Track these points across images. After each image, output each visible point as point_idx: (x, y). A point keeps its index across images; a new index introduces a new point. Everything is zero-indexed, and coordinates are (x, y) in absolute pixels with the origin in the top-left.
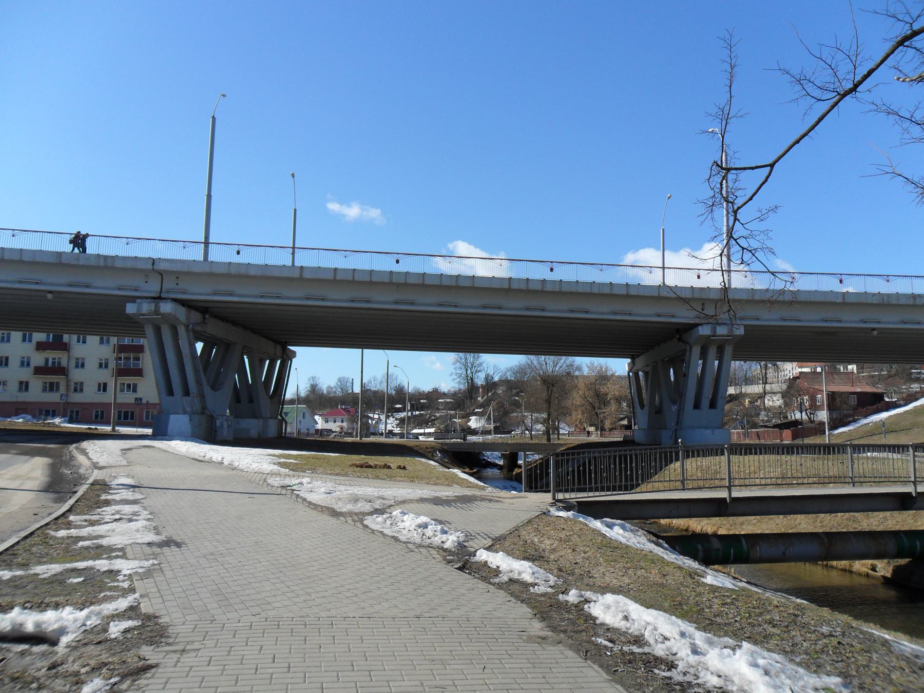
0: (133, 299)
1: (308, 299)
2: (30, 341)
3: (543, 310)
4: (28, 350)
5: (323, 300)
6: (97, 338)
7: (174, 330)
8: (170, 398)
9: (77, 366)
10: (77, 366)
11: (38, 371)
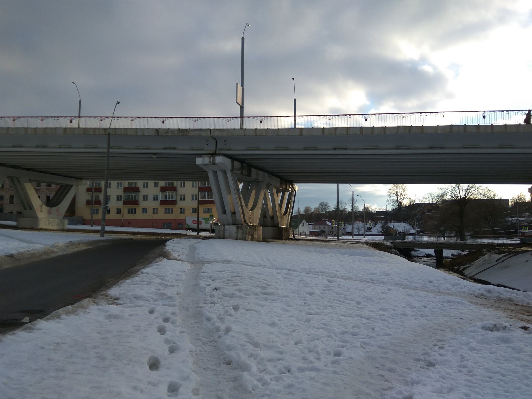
0: (200, 155)
1: (305, 149)
2: (158, 186)
3: (477, 148)
4: (156, 191)
5: (345, 149)
6: (191, 183)
7: (224, 172)
8: (224, 215)
9: (181, 199)
10: (181, 199)
11: (162, 203)
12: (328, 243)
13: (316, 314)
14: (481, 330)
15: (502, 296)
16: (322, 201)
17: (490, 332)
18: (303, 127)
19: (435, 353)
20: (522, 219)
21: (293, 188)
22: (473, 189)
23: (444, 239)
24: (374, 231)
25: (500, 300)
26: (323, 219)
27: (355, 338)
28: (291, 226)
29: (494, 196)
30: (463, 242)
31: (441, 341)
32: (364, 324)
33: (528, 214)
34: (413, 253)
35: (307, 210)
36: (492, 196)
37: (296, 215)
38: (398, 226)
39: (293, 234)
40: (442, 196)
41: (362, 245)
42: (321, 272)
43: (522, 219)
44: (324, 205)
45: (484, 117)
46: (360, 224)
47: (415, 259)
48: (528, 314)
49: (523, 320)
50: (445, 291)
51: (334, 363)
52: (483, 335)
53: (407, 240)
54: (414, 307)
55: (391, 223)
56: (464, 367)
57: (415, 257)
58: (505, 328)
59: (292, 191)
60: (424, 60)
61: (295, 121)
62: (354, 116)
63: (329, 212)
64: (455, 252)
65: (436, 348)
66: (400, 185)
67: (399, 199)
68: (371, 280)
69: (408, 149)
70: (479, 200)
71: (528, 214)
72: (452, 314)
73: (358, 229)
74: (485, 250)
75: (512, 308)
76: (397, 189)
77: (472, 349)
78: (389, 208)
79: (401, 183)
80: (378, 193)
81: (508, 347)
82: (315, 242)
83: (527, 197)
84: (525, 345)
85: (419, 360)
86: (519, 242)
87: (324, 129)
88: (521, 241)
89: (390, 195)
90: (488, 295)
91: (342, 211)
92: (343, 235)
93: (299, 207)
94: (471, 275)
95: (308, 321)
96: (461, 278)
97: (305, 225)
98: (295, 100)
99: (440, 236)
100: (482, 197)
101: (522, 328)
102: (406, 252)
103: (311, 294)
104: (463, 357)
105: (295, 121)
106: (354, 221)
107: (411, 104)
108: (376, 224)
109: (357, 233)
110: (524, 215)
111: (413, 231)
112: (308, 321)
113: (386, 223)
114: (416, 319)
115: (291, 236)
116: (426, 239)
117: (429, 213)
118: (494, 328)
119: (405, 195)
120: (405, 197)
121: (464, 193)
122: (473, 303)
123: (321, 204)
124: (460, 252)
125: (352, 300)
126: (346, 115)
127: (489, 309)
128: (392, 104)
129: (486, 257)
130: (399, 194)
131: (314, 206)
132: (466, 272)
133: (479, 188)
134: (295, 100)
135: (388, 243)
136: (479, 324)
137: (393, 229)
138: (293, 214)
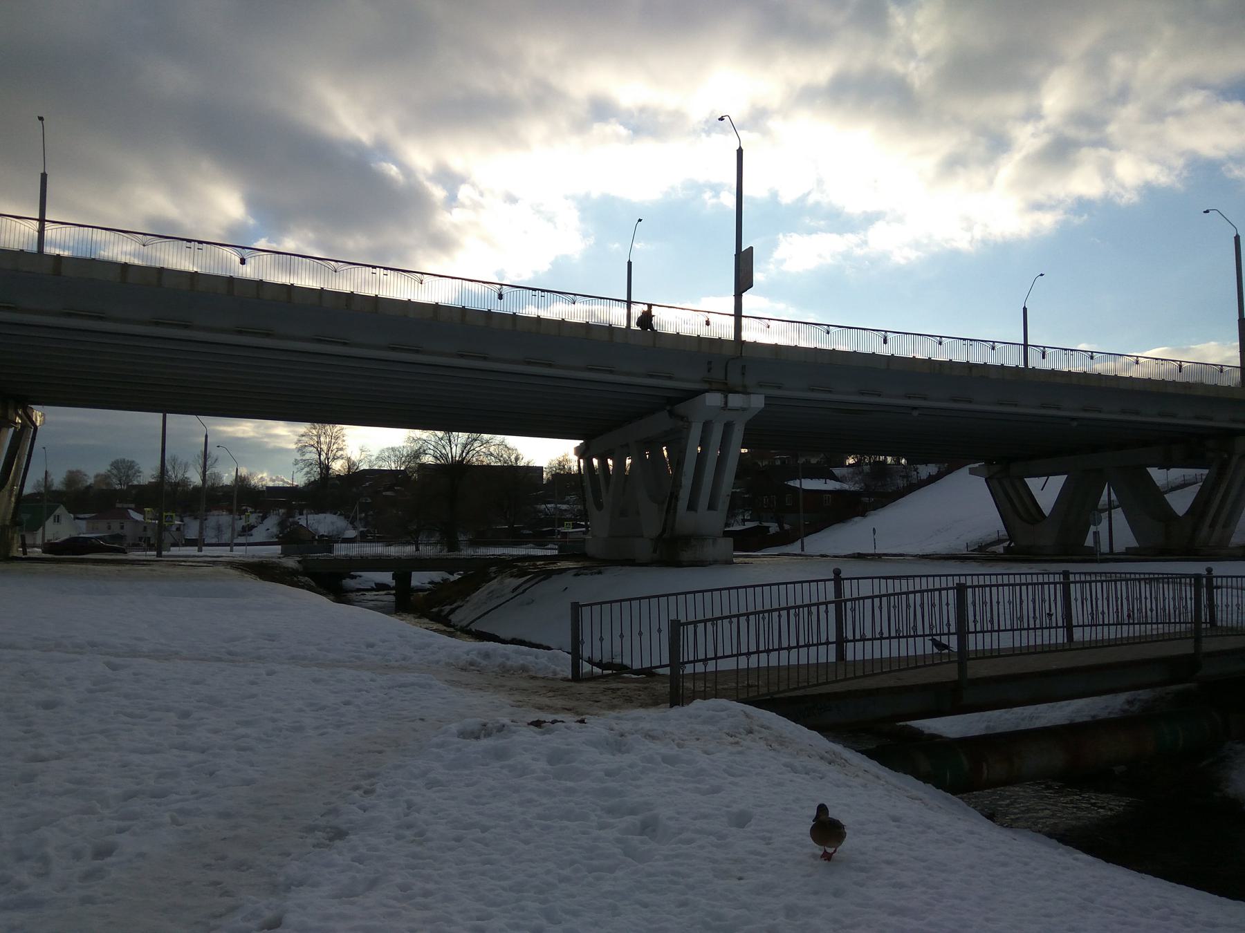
12: (127, 567)
13: (57, 758)
14: (457, 740)
15: (509, 663)
16: (119, 457)
17: (474, 742)
18: (66, 253)
19: (354, 807)
20: (564, 507)
21: (30, 419)
22: (476, 444)
23: (417, 549)
24: (259, 534)
25: (505, 671)
26: (118, 505)
27: (159, 805)
28: (16, 522)
29: (517, 459)
30: (454, 555)
31: (371, 776)
32: (190, 765)
33: (574, 497)
34: (348, 583)
35: (73, 478)
36: (513, 458)
37: (39, 494)
38: (319, 522)
39: (24, 546)
40: (417, 454)
41: (221, 568)
42: (93, 645)
43: (564, 507)
44: (124, 468)
45: (500, 296)
46: (224, 518)
47: (353, 596)
48: (551, 694)
49: (540, 708)
50: (397, 664)
51: (87, 876)
52: (459, 750)
53: (336, 553)
54: (323, 708)
55: (301, 514)
56: (409, 827)
57: (352, 591)
58: (502, 728)
59: (24, 426)
60: (384, 149)
61: (41, 231)
62: (213, 247)
63: (139, 487)
64: (437, 576)
65: (356, 794)
66: (328, 427)
67: (323, 458)
68: (230, 653)
69: (345, 344)
70: (489, 466)
71: (574, 497)
72: (404, 713)
73: (219, 529)
74: (493, 569)
75: (524, 684)
76: (319, 436)
77: (431, 785)
78: (300, 480)
79: (329, 423)
80: (273, 443)
81: (502, 767)
82: (91, 567)
83: (574, 463)
84: (533, 759)
85: (311, 829)
86: (556, 552)
87: (125, 266)
88: (560, 550)
89: (302, 450)
90: (484, 663)
91: (177, 484)
92: (174, 545)
93: (46, 469)
94: (465, 623)
95: (29, 778)
96: (435, 631)
97: (63, 520)
98: (44, 177)
99: (409, 543)
100: (493, 462)
101: (532, 723)
102: (332, 581)
103: (48, 705)
104: (410, 805)
105: (41, 231)
106: (208, 510)
107: (355, 243)
108: (264, 518)
109: (214, 541)
110: (568, 498)
111: (351, 533)
112: (29, 778)
113: (290, 514)
114: (322, 734)
115: (17, 551)
116: (379, 549)
117: (388, 493)
118: (484, 731)
119: (338, 449)
120: (340, 453)
121: (459, 451)
122: (452, 683)
123: (116, 465)
124: (446, 575)
125: (168, 711)
126: (189, 241)
127: (482, 693)
128: (311, 235)
129: (494, 584)
130: (325, 447)
131: (93, 470)
132: (454, 618)
133: (487, 442)
134: (44, 177)
135: (291, 562)
136: (454, 727)
137: (306, 529)
138: (27, 490)
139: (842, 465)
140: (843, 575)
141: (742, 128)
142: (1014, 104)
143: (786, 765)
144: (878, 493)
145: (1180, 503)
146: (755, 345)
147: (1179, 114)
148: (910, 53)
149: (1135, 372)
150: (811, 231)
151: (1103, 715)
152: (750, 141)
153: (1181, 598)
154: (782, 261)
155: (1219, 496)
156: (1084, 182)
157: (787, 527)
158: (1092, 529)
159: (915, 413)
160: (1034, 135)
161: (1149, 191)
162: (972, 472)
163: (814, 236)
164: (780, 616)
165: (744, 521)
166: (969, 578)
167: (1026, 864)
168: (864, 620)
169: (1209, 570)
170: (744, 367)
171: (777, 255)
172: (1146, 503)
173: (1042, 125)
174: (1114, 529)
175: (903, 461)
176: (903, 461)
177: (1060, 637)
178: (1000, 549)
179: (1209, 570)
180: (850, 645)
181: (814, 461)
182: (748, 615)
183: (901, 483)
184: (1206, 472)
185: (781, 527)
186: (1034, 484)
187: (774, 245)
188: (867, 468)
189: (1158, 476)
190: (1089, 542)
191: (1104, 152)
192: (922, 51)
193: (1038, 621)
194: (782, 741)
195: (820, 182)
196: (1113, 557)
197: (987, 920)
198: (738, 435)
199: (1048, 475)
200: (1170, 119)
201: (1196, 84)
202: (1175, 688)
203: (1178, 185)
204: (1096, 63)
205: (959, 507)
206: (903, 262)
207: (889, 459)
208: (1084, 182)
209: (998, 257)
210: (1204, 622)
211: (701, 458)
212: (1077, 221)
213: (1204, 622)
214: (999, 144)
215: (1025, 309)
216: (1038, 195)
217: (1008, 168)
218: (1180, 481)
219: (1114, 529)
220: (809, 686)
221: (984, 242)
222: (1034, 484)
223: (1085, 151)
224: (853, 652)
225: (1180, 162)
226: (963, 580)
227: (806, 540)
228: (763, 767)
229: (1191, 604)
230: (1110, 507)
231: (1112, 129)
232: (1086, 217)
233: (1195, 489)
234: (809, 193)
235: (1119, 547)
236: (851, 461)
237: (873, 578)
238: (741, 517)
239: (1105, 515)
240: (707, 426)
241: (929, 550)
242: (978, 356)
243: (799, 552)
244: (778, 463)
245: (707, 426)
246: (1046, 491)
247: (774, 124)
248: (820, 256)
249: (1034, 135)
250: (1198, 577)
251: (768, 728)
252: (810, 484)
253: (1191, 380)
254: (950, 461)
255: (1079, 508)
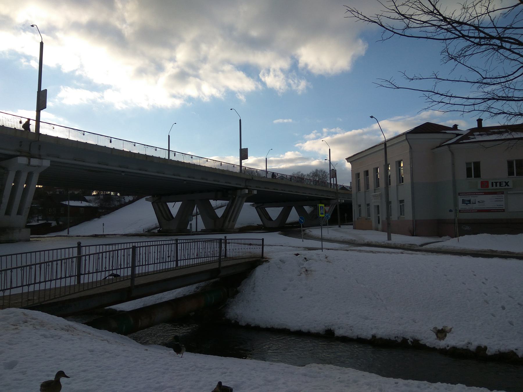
139: (90, 195)
140: (82, 245)
141: (43, 33)
142: (165, 53)
143: (41, 335)
144: (107, 207)
145: (220, 213)
146: (46, 136)
147: (223, 71)
148: (124, 21)
149: (207, 165)
150: (77, 87)
151: (188, 294)
152: (46, 38)
153: (205, 248)
154: (62, 99)
155: (231, 212)
156: (190, 90)
157: (61, 223)
158: (190, 222)
159: (123, 174)
160: (173, 67)
161: (213, 98)
162: (147, 200)
163: (78, 90)
164: (57, 264)
165: (38, 220)
166: (136, 244)
167: (145, 360)
168: (90, 265)
169: (225, 237)
170: (40, 146)
171: (60, 95)
172: (208, 212)
173: (176, 64)
174: (198, 223)
175: (118, 194)
176: (118, 194)
177: (173, 265)
178: (156, 231)
179: (225, 237)
180: (137, 268)
181: (76, 193)
182: (40, 264)
183: (117, 204)
184: (228, 202)
185: (58, 223)
186: (170, 205)
187: (59, 90)
188: (102, 197)
189: (213, 203)
190: (188, 228)
191: (198, 80)
192: (129, 20)
193: (158, 260)
194: (42, 324)
195: (82, 66)
196: (197, 233)
197: (124, 387)
198: (35, 178)
199: (175, 202)
200: (220, 73)
201: (228, 62)
202: (212, 281)
203: (223, 98)
204: (196, 45)
205: (141, 214)
206: (120, 109)
207: (112, 193)
208: (190, 90)
209: (158, 114)
210: (222, 257)
211: (14, 189)
212: (188, 105)
213: (222, 257)
214: (160, 68)
215: (169, 136)
216: (174, 92)
217: (163, 78)
218: (220, 205)
219: (198, 223)
220: (60, 297)
221: (153, 106)
222: (170, 205)
223: (191, 79)
224: (85, 279)
225: (223, 90)
226: (134, 244)
227: (71, 229)
228: (29, 338)
229: (217, 249)
230: (197, 214)
231: (201, 72)
232: (191, 103)
233: (224, 208)
234: (77, 70)
235: (199, 230)
236: (94, 193)
237: (96, 245)
238: (37, 218)
239: (194, 218)
240: (18, 174)
241: (127, 232)
242: (150, 152)
243: (66, 234)
244: (58, 193)
245: (18, 174)
246: (174, 208)
247: (59, 35)
248: (81, 99)
249: (173, 67)
250: (221, 240)
251: (35, 319)
252: (73, 203)
253: (225, 169)
254: (138, 196)
255: (185, 214)
